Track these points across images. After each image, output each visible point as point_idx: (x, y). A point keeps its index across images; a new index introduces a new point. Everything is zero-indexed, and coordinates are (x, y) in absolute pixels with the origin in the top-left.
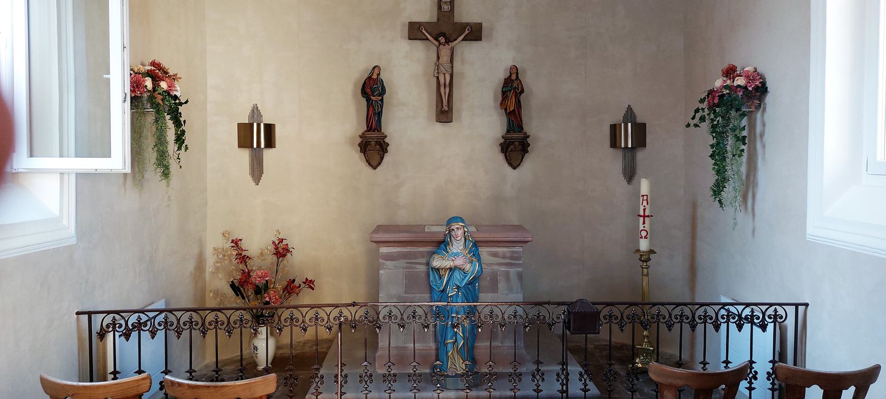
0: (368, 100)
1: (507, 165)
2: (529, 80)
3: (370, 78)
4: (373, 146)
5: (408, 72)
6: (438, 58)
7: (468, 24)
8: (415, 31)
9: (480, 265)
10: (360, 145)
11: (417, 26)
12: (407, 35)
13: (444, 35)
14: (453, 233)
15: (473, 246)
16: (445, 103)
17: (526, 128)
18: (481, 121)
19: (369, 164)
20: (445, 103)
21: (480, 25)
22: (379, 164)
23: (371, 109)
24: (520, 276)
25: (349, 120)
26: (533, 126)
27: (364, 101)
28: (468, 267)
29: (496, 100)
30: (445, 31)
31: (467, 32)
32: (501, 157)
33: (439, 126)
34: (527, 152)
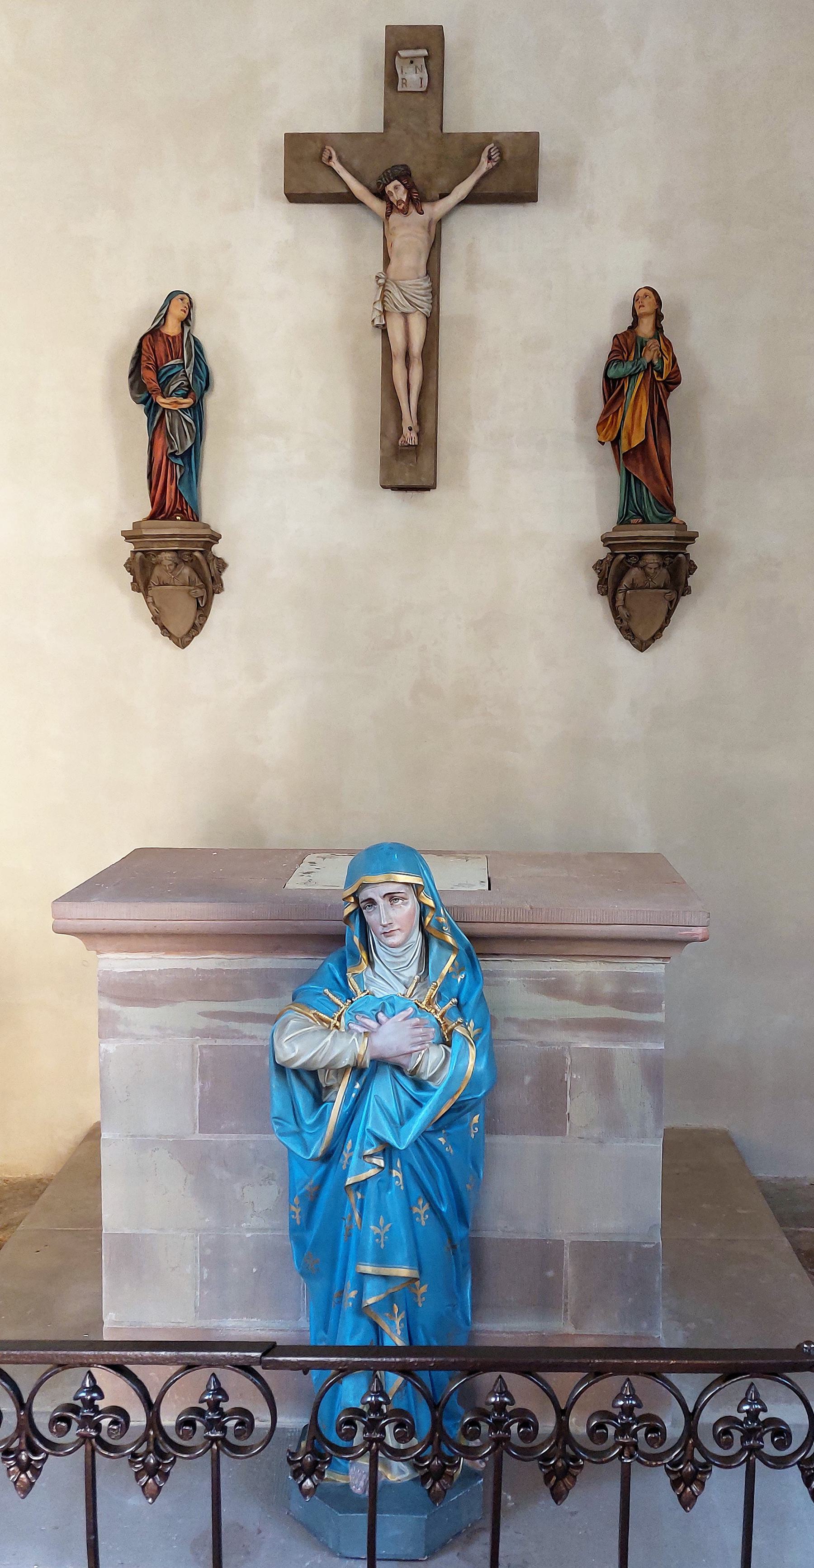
0: (151, 408)
1: (615, 634)
2: (698, 343)
3: (155, 333)
4: (176, 564)
5: (286, 308)
6: (387, 260)
7: (488, 137)
8: (312, 171)
9: (491, 1051)
10: (129, 566)
11: (315, 148)
12: (375, 473)
13: (404, 175)
14: (371, 917)
15: (458, 968)
16: (409, 419)
17: (683, 513)
18: (534, 488)
19: (165, 630)
20: (409, 419)
21: (531, 140)
22: (196, 629)
23: (160, 442)
24: (654, 1073)
25: (112, 492)
26: (707, 500)
27: (139, 411)
28: (431, 1059)
29: (582, 413)
30: (414, 162)
31: (484, 166)
32: (597, 609)
33: (393, 503)
34: (687, 590)
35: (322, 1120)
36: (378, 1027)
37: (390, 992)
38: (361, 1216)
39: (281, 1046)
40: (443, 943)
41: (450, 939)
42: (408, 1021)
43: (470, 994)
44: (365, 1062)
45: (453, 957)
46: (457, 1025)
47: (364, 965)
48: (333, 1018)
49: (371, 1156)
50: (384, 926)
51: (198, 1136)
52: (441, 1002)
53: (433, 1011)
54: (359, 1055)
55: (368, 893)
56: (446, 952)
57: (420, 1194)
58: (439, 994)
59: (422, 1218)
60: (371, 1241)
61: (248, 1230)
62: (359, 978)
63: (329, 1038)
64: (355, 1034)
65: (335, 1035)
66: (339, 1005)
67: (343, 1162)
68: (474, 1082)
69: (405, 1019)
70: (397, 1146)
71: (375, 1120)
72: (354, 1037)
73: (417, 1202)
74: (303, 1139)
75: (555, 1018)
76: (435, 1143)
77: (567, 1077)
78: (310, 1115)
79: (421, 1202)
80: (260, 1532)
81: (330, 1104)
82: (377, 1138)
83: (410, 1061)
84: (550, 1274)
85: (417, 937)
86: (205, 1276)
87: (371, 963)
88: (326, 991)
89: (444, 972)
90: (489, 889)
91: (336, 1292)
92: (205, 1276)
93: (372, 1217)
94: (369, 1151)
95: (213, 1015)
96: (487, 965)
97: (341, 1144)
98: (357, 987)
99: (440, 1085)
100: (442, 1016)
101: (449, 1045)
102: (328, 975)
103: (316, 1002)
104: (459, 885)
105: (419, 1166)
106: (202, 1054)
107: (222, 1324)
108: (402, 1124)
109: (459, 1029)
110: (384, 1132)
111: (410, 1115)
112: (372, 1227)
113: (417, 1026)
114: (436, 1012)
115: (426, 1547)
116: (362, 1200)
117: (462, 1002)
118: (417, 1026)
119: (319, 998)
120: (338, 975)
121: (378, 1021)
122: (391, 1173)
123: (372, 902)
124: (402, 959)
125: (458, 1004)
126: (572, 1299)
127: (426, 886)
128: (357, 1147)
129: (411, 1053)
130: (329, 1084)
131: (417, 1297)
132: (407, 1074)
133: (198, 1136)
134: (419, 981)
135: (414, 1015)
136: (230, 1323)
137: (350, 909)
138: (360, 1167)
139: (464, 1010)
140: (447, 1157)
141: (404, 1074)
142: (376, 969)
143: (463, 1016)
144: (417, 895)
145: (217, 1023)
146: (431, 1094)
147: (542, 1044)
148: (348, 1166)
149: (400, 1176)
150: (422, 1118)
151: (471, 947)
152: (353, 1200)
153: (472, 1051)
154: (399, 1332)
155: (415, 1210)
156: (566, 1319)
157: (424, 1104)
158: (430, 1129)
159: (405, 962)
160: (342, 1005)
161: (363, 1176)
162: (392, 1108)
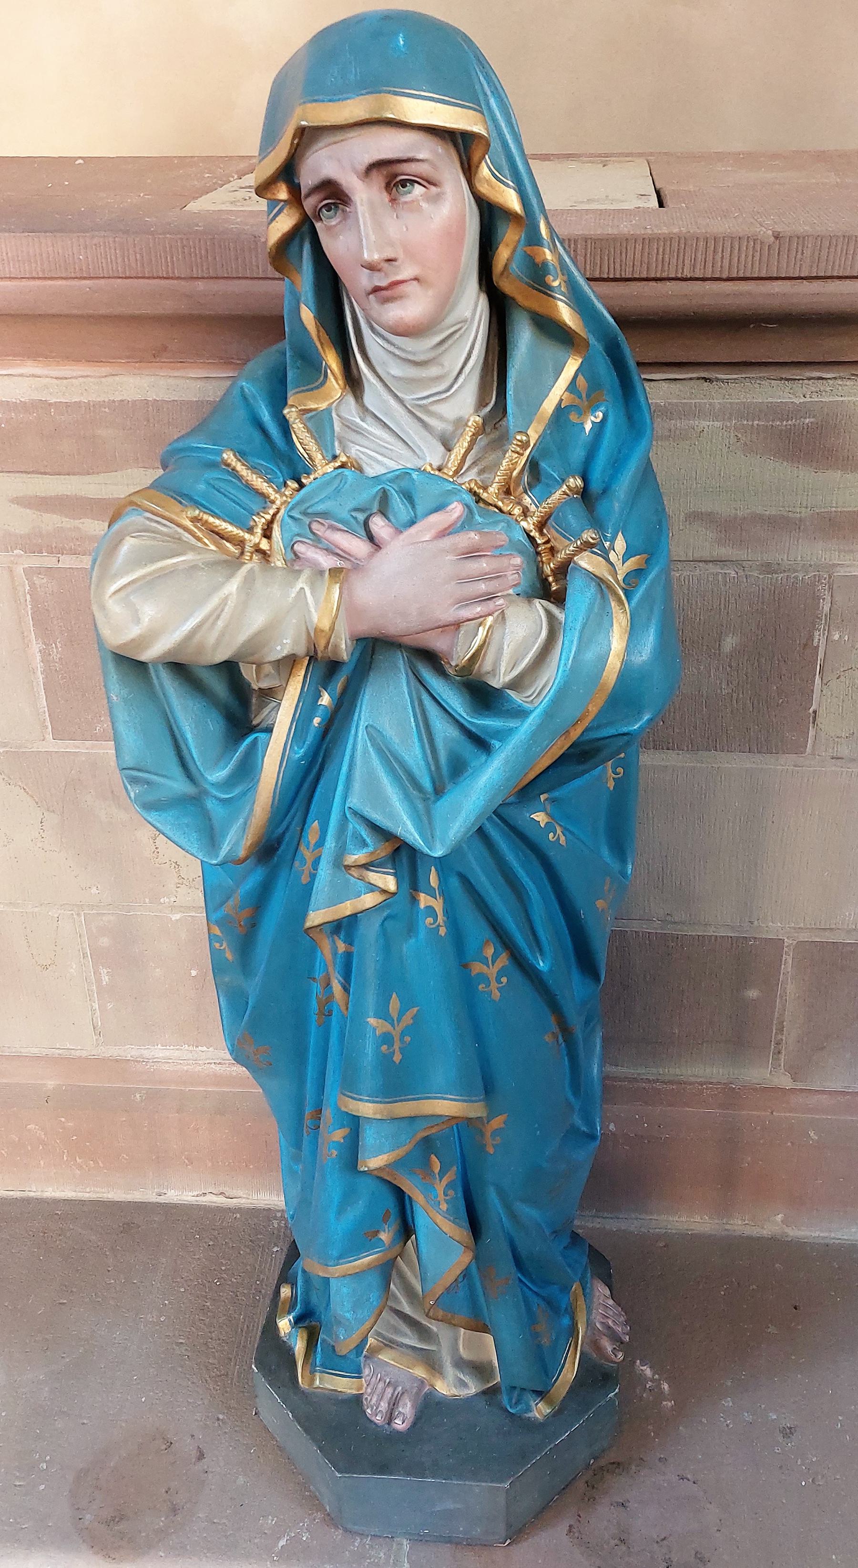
14: (338, 244)
15: (585, 394)
28: (511, 637)
35: (247, 770)
36: (371, 555)
37: (404, 460)
38: (346, 989)
39: (103, 607)
40: (550, 328)
41: (566, 314)
42: (447, 542)
43: (617, 464)
44: (336, 647)
45: (572, 365)
46: (580, 550)
47: (335, 385)
48: (250, 530)
49: (366, 866)
50: (372, 267)
51: (51, 745)
52: (538, 489)
53: (517, 511)
54: (318, 631)
55: (321, 164)
56: (551, 350)
57: (487, 933)
58: (533, 466)
59: (494, 985)
60: (369, 1049)
61: (173, 908)
62: (320, 424)
63: (233, 586)
64: (306, 573)
65: (249, 580)
66: (264, 496)
67: (301, 867)
68: (624, 696)
69: (444, 533)
70: (426, 850)
71: (371, 785)
72: (302, 583)
73: (481, 949)
74: (206, 816)
75: (805, 513)
76: (520, 823)
77: (819, 639)
78: (216, 764)
79: (490, 951)
80: (201, 1456)
81: (262, 736)
82: (374, 828)
83: (453, 645)
84: (753, 993)
85: (473, 307)
86: (105, 979)
87: (353, 382)
88: (229, 456)
89: (549, 405)
90: (661, 205)
91: (308, 1110)
92: (105, 979)
93: (371, 999)
94: (357, 856)
95: (44, 504)
96: (659, 391)
97: (295, 827)
98: (312, 446)
99: (538, 698)
100: (541, 526)
101: (559, 599)
102: (241, 414)
103: (202, 487)
104: (589, 201)
105: (483, 878)
106: (32, 585)
107: (146, 1053)
108: (439, 791)
109: (585, 561)
110: (392, 816)
111: (458, 769)
112: (372, 1021)
113: (472, 554)
114: (525, 513)
115: (509, 1526)
116: (348, 955)
117: (596, 486)
118: (472, 554)
119: (215, 474)
120: (266, 416)
121: (371, 538)
122: (414, 900)
123: (334, 195)
124: (433, 371)
125: (585, 494)
126: (791, 1036)
127: (495, 144)
128: (330, 843)
129: (457, 625)
130: (264, 685)
131: (482, 1135)
132: (451, 672)
133: (51, 745)
134: (481, 430)
135: (467, 523)
136: (158, 1052)
137: (285, 223)
138: (344, 888)
139: (602, 507)
140: (551, 853)
141: (441, 672)
142: (369, 399)
143: (598, 524)
144: (469, 170)
145: (51, 521)
146: (512, 724)
147: (768, 568)
148: (313, 877)
149: (438, 905)
150: (487, 780)
151: (621, 337)
152: (328, 955)
153: (620, 621)
154: (444, 1207)
155: (477, 968)
156: (776, 1066)
157: (496, 744)
158: (512, 799)
159: (438, 379)
160: (273, 495)
161: (347, 908)
162: (414, 755)
